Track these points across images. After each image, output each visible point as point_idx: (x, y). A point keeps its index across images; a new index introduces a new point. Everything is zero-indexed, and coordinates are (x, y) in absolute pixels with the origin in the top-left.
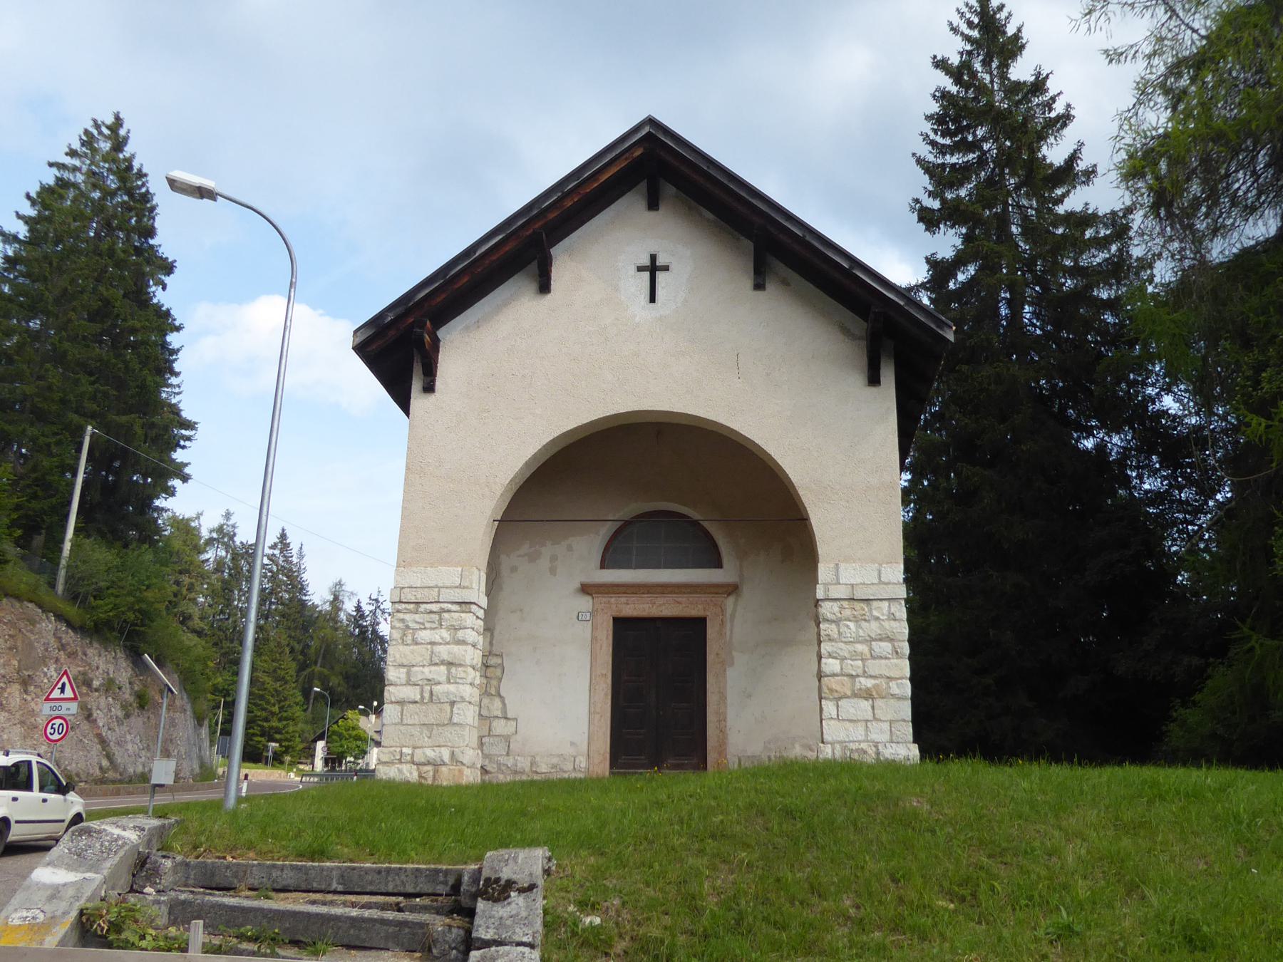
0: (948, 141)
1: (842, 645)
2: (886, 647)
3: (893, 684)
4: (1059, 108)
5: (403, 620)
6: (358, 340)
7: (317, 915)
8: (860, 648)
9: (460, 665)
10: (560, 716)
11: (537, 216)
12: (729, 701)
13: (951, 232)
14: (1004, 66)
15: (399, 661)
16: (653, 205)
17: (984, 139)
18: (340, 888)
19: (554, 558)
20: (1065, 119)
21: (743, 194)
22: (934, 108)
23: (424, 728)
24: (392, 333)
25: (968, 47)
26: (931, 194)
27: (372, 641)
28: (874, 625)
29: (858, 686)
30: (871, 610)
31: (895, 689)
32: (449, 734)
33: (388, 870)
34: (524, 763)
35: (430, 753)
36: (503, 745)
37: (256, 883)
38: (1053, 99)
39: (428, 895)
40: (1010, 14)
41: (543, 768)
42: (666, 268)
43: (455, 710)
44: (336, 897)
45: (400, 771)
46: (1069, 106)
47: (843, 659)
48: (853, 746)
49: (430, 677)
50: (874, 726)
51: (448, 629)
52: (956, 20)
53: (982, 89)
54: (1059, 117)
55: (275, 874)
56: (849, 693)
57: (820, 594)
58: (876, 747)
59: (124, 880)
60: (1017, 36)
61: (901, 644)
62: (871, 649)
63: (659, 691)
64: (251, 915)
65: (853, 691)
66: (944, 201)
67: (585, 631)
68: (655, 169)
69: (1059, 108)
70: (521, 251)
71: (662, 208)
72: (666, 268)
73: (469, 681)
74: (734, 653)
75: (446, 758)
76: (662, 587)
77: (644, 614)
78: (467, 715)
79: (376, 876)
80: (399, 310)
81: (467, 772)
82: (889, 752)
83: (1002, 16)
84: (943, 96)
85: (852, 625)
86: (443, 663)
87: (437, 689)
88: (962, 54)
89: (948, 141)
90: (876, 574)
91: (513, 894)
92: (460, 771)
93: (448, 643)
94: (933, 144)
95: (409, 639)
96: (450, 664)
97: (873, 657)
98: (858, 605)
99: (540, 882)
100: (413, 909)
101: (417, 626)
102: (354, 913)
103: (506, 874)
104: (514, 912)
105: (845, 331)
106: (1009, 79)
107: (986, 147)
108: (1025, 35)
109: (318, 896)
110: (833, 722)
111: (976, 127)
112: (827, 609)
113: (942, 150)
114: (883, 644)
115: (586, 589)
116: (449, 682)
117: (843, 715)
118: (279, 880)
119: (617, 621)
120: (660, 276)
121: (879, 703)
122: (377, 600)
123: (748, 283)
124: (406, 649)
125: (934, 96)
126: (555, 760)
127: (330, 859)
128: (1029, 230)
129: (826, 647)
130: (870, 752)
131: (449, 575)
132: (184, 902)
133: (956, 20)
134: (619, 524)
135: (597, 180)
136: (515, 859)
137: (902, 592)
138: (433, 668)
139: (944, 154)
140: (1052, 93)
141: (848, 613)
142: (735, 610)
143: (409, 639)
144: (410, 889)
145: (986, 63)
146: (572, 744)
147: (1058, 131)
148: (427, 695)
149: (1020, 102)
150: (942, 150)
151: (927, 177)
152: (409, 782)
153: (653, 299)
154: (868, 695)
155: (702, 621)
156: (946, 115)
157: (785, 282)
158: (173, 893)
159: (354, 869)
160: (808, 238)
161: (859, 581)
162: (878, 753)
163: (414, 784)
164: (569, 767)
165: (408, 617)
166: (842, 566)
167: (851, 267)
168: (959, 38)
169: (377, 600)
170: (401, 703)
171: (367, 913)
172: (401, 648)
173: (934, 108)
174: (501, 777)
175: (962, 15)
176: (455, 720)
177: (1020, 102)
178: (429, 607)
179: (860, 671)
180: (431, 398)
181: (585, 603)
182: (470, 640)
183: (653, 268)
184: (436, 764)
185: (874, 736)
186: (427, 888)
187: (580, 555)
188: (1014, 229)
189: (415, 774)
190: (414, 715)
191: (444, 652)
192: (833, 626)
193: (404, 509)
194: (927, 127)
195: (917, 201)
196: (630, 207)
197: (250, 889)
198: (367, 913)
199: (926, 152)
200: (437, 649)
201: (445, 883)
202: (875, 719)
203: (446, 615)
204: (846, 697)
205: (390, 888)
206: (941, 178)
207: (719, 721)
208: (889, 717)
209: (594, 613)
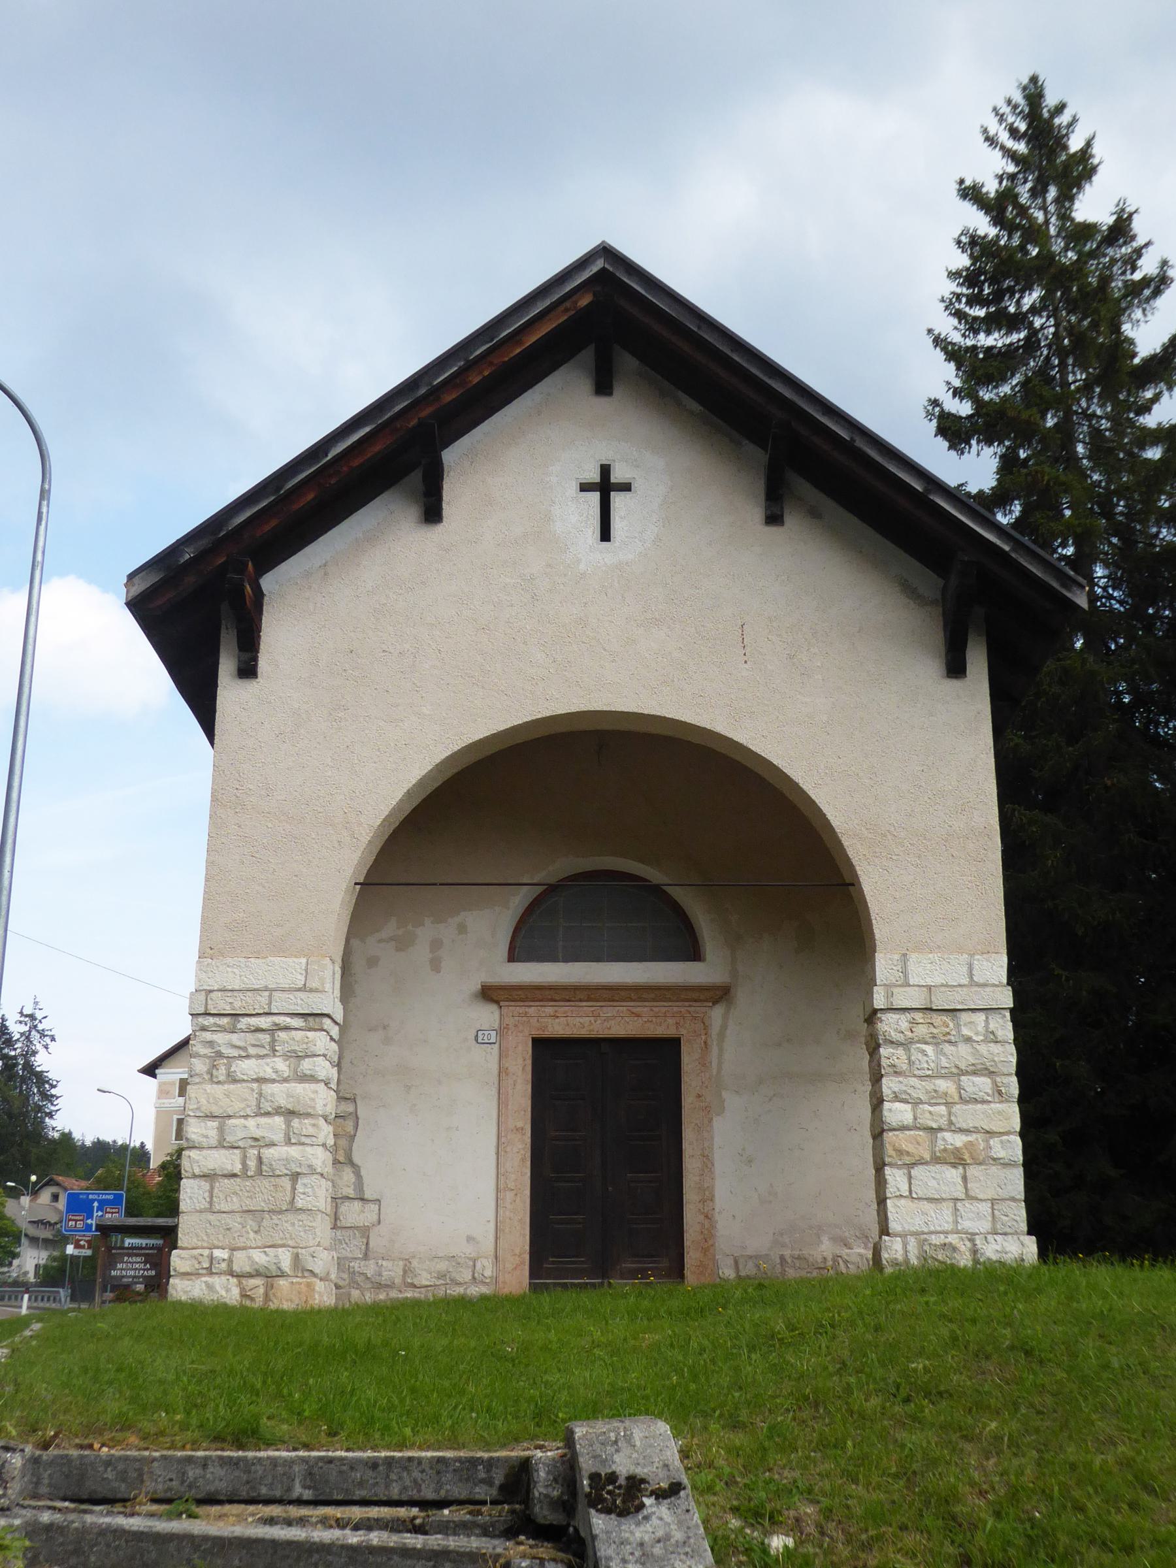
0: (980, 312)
1: (913, 1081)
2: (981, 1085)
3: (994, 1142)
4: (1148, 266)
5: (211, 1043)
6: (137, 589)
7: (290, 1543)
8: (943, 1085)
9: (308, 1115)
10: (453, 1195)
11: (425, 397)
12: (718, 1168)
13: (988, 451)
14: (1066, 198)
15: (206, 1108)
16: (603, 387)
17: (1034, 310)
18: (308, 1495)
19: (436, 944)
20: (1159, 284)
21: (754, 371)
22: (962, 261)
23: (249, 1217)
24: (191, 581)
25: (1011, 168)
26: (957, 393)
27: (23, 1080)
28: (964, 1049)
29: (940, 1145)
30: (958, 1026)
31: (998, 1151)
32: (290, 1225)
33: (389, 1462)
34: (392, 1271)
35: (260, 1258)
36: (359, 1242)
37: (160, 1489)
38: (1138, 252)
39: (461, 1503)
40: (1074, 120)
41: (424, 1279)
42: (626, 487)
43: (300, 1188)
44: (304, 1511)
45: (210, 1287)
46: (1164, 263)
47: (917, 1103)
48: (936, 1240)
49: (258, 1133)
50: (965, 1207)
51: (286, 1056)
52: (994, 127)
53: (1034, 233)
54: (1146, 282)
55: (192, 1473)
56: (927, 1157)
57: (879, 1001)
58: (972, 1240)
59: (276, 1524)
60: (1085, 154)
61: (1006, 1080)
62: (960, 1088)
63: (606, 1152)
64: (172, 1547)
65: (933, 1153)
66: (978, 403)
67: (488, 1058)
68: (612, 331)
69: (1148, 266)
70: (393, 455)
71: (618, 391)
72: (626, 487)
73: (321, 1140)
74: (725, 1094)
75: (286, 1264)
76: (609, 990)
77: (583, 1033)
78: (315, 1194)
79: (370, 1473)
80: (203, 543)
81: (319, 1286)
82: (991, 1250)
83: (1063, 119)
84: (973, 243)
85: (929, 1049)
86: (278, 1111)
87: (268, 1153)
88: (1001, 178)
89: (980, 312)
90: (965, 969)
91: (648, 1501)
92: (309, 1285)
93: (286, 1080)
94: (959, 315)
95: (221, 1074)
96: (290, 1113)
97: (963, 1101)
98: (938, 1019)
99: (685, 1481)
100: (445, 1528)
101: (235, 1053)
102: (354, 1538)
103: (623, 1465)
104: (660, 1533)
105: (909, 590)
106: (1073, 220)
107: (1038, 322)
108: (1098, 152)
109: (275, 1510)
110: (903, 1201)
111: (1022, 291)
112: (889, 1025)
113: (973, 325)
114: (978, 1080)
115: (489, 994)
116: (288, 1142)
117: (919, 1191)
118: (201, 1482)
119: (540, 1044)
120: (617, 499)
121: (973, 1171)
122: (32, 1017)
123: (755, 513)
124: (218, 1090)
125: (959, 242)
126: (442, 1266)
127: (269, 1445)
128: (1100, 449)
129: (889, 1085)
130: (963, 1248)
131: (286, 970)
132: (49, 1528)
133: (994, 127)
134: (540, 889)
135: (520, 343)
136: (629, 1439)
137: (1006, 998)
138: (263, 1120)
139: (976, 332)
140: (1140, 241)
141: (922, 1030)
142: (724, 1027)
143: (221, 1074)
144: (429, 1494)
145: (1038, 192)
146: (470, 1239)
147: (1148, 300)
148: (252, 1164)
149: (1093, 254)
150: (973, 325)
151: (952, 366)
152: (225, 1304)
153: (605, 535)
154: (956, 1159)
155: (673, 1044)
156: (979, 272)
157: (814, 513)
158: (28, 1514)
159: (330, 1461)
160: (860, 443)
161: (939, 980)
162: (975, 1252)
163: (234, 1307)
164: (467, 1276)
165: (220, 1038)
166: (913, 957)
167: (927, 490)
168: (998, 154)
169: (32, 1017)
170: (209, 1177)
171: (376, 1538)
172: (208, 1087)
173: (962, 261)
174: (355, 1294)
175: (1002, 118)
176: (300, 1203)
177: (1093, 254)
178: (254, 1021)
179: (943, 1122)
180: (249, 689)
181: (488, 1016)
182: (322, 1075)
183: (605, 487)
184: (270, 1276)
185: (966, 1224)
186: (458, 1491)
187: (476, 940)
188: (1080, 449)
189: (236, 1292)
190: (230, 1196)
191: (279, 1094)
192: (900, 1051)
193: (210, 864)
194: (950, 287)
195: (935, 403)
196: (563, 395)
197: (155, 1501)
198: (376, 1538)
199: (949, 328)
200: (268, 1089)
201: (489, 1482)
202: (969, 1197)
203: (282, 1035)
204: (921, 1162)
205: (395, 1492)
206: (976, 369)
207: (703, 1201)
208: (990, 1194)
209: (502, 1031)
